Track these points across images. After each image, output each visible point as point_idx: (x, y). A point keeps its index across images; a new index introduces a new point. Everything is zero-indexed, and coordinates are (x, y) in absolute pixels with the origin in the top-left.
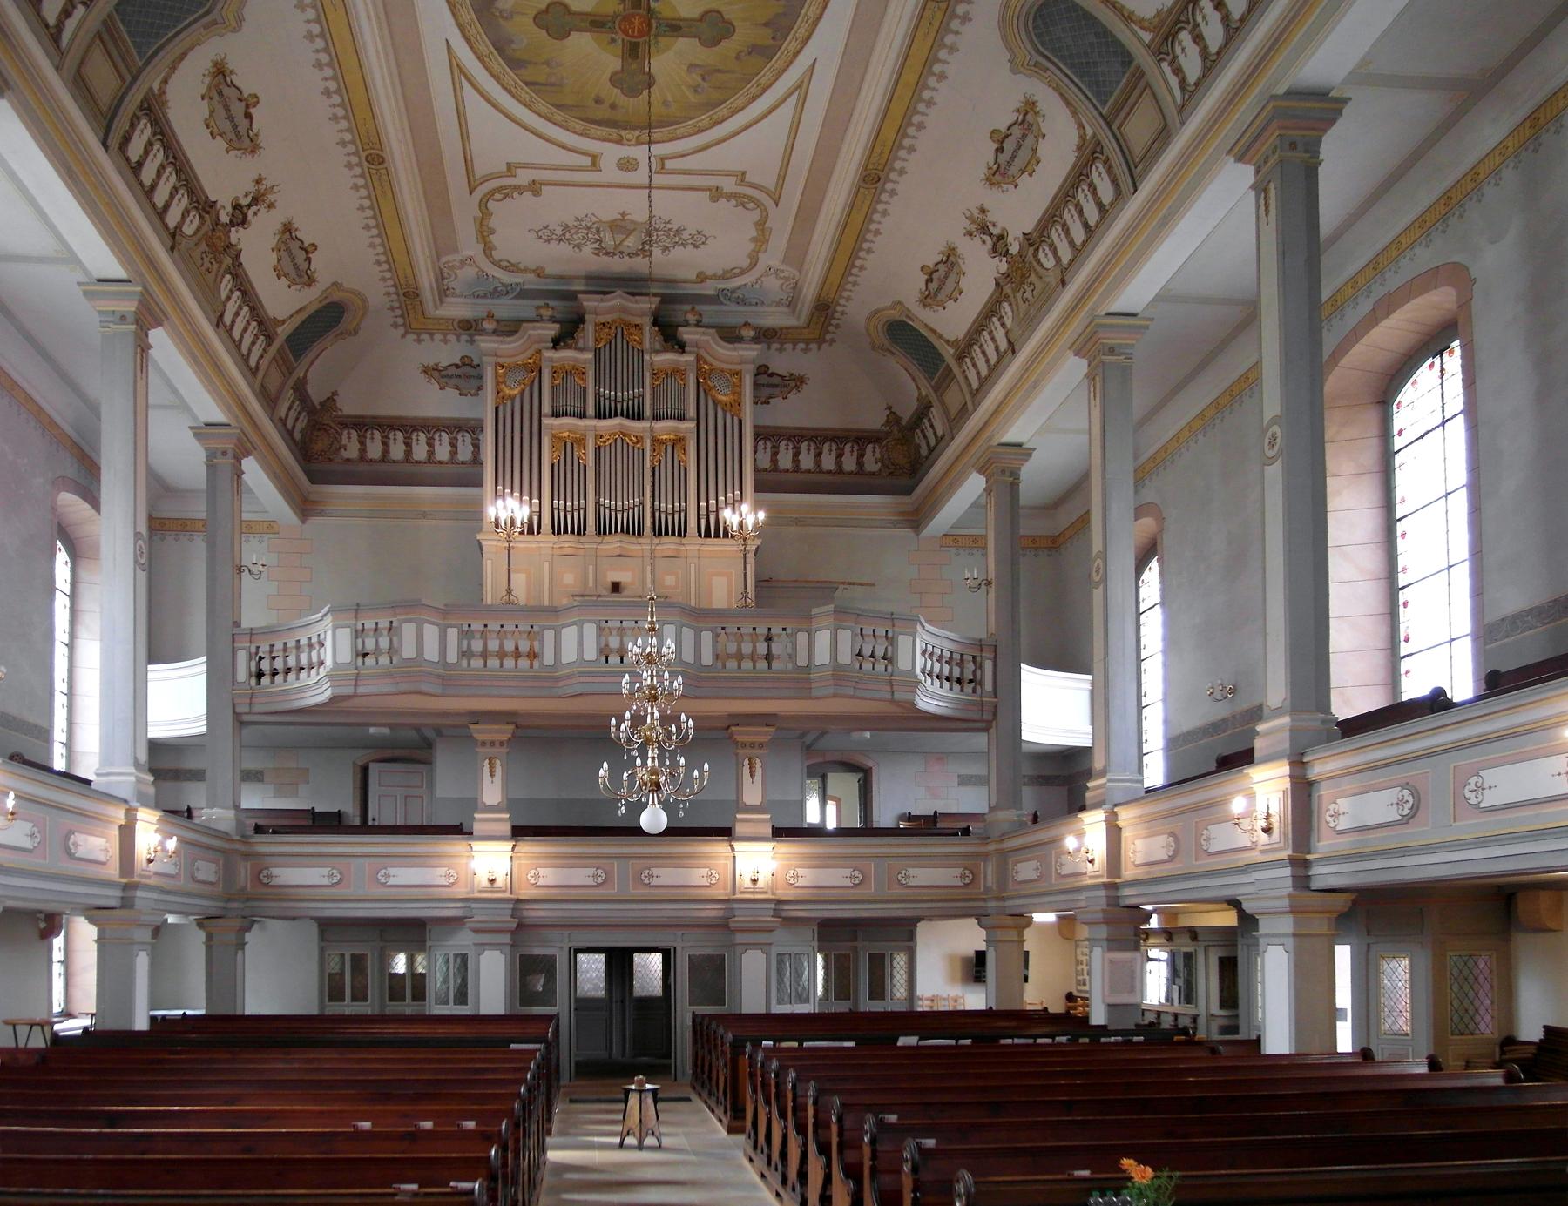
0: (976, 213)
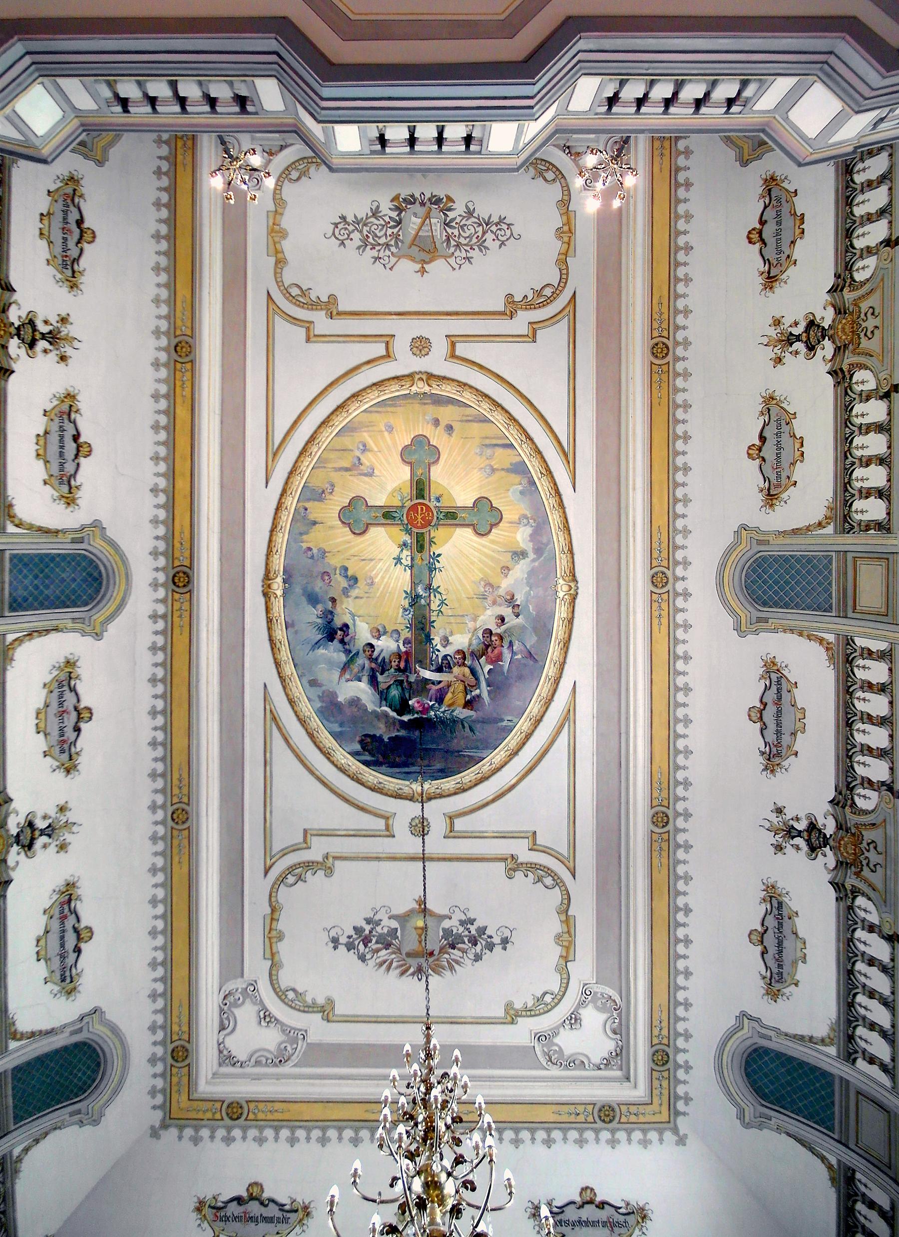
0: (69, 351)
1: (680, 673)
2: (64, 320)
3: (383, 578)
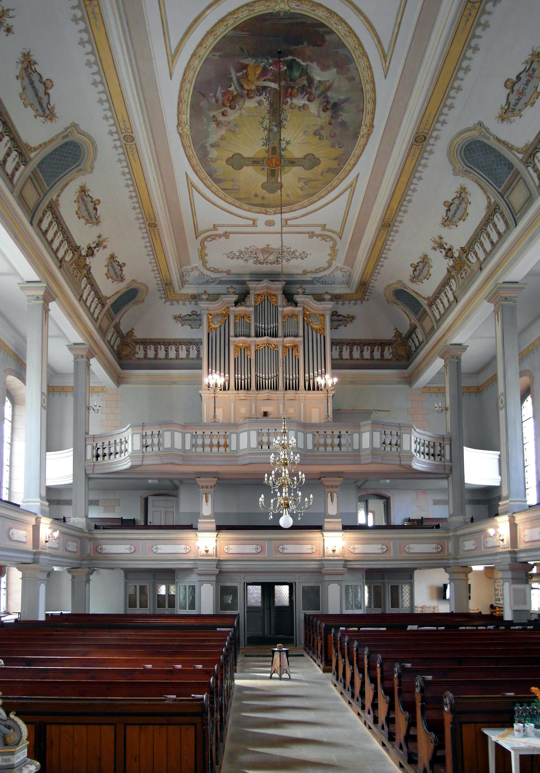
1: (102, 92)
2: (434, 249)
3: (298, 135)
